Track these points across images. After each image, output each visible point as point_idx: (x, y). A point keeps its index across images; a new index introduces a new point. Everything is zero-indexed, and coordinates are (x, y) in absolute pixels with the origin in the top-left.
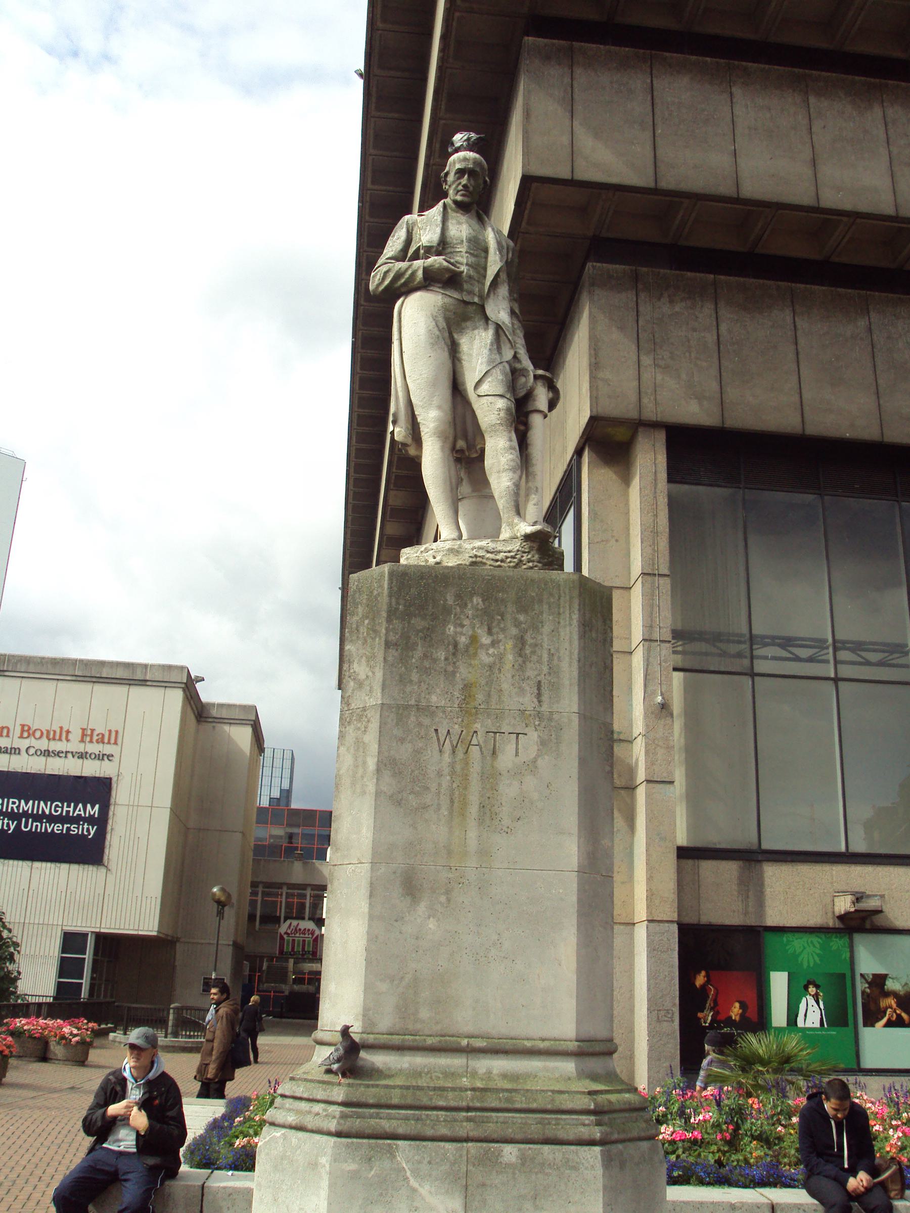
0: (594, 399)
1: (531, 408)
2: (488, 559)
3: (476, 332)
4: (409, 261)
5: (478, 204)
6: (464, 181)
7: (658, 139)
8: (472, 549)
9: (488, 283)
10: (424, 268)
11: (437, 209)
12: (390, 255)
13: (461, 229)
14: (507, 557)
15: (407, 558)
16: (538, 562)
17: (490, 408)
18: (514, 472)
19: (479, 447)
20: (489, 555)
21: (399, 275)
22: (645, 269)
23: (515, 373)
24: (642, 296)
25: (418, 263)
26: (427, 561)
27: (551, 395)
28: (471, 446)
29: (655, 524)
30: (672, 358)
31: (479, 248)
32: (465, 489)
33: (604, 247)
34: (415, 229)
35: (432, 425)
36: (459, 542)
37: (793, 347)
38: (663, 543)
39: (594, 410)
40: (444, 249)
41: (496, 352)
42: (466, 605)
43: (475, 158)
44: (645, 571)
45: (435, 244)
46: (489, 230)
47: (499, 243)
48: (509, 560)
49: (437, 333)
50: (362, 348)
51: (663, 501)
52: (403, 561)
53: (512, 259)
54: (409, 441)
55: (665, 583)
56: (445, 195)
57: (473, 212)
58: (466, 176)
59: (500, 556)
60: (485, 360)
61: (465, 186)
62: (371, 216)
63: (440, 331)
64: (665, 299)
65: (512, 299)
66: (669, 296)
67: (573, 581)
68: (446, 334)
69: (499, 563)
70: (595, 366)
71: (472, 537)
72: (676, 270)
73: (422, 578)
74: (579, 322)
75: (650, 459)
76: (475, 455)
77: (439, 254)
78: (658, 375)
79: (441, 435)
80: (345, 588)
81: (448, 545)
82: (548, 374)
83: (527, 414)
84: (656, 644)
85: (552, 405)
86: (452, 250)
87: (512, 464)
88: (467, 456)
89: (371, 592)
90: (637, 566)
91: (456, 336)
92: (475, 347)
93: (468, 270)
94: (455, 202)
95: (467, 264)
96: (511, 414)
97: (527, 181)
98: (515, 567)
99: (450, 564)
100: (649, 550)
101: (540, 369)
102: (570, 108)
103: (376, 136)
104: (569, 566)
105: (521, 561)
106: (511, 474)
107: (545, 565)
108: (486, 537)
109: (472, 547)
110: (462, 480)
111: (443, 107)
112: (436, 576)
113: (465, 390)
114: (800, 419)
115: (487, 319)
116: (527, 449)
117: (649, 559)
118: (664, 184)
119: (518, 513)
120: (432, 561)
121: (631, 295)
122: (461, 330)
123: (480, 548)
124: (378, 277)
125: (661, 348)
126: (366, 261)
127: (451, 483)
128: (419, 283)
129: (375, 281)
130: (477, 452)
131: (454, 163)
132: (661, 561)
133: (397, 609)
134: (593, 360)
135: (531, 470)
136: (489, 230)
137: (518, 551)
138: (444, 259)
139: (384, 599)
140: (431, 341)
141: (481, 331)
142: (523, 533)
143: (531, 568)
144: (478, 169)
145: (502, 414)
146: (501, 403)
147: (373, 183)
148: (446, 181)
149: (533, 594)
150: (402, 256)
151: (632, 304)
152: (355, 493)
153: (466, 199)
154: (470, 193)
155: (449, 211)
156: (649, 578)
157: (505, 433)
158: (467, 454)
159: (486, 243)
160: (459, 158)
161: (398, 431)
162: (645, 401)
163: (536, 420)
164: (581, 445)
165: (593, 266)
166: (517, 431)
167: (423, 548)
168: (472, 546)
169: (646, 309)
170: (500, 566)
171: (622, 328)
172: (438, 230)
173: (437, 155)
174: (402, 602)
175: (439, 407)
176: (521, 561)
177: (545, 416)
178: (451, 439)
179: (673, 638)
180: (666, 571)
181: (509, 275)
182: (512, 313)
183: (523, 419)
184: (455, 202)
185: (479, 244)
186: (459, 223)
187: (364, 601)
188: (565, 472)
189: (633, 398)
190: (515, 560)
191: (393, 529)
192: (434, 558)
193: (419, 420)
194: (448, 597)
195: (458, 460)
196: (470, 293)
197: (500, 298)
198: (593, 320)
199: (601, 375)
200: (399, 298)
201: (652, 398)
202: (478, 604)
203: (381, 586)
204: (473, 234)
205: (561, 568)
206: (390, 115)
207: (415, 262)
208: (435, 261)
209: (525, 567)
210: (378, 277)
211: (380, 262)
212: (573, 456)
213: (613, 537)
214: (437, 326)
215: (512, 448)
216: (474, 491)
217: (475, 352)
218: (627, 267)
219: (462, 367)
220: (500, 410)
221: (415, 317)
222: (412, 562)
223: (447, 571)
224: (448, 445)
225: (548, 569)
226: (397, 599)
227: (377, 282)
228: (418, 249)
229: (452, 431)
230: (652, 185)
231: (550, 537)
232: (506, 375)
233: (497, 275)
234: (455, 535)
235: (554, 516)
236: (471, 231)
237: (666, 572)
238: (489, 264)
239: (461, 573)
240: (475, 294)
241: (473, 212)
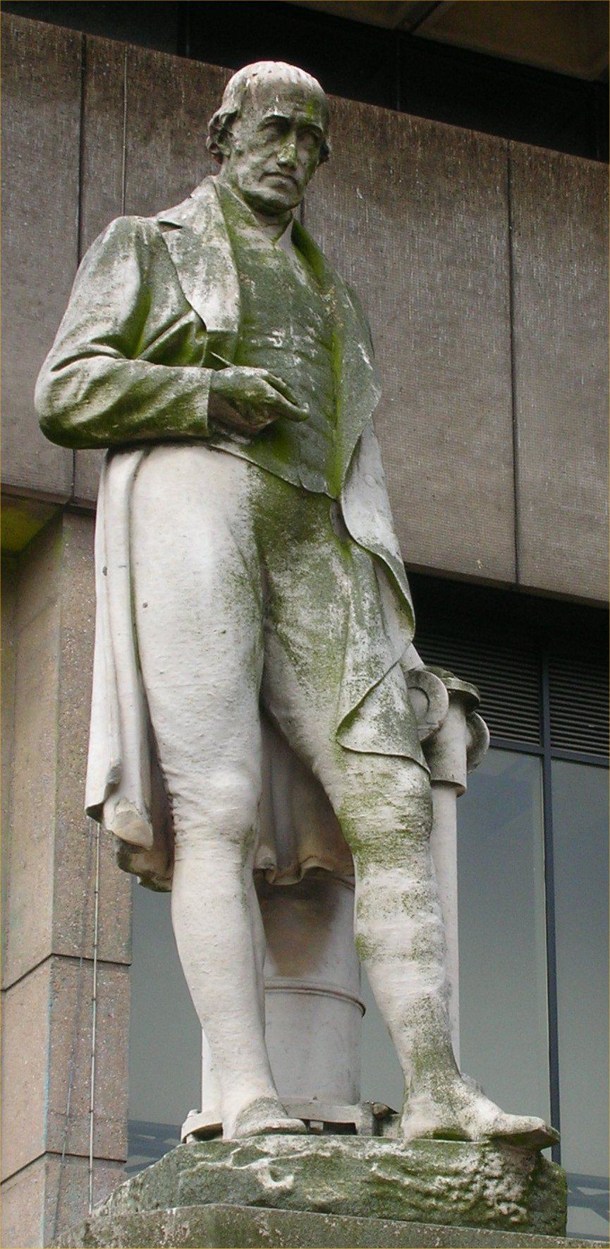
10: (214, 393)
14: (451, 1188)
16: (520, 1203)
20: (407, 1181)
22: (107, 42)
24: (99, 122)
35: (219, 810)
37: (504, 327)
48: (454, 1195)
49: (242, 570)
59: (437, 1184)
64: (161, 144)
72: (193, 57)
84: (83, 1166)
91: (276, 578)
114: (508, 541)
121: (66, 114)
137: (476, 1172)
151: (69, 146)
156: (70, 969)
175: (241, 765)
179: (132, 1151)
190: (469, 1196)
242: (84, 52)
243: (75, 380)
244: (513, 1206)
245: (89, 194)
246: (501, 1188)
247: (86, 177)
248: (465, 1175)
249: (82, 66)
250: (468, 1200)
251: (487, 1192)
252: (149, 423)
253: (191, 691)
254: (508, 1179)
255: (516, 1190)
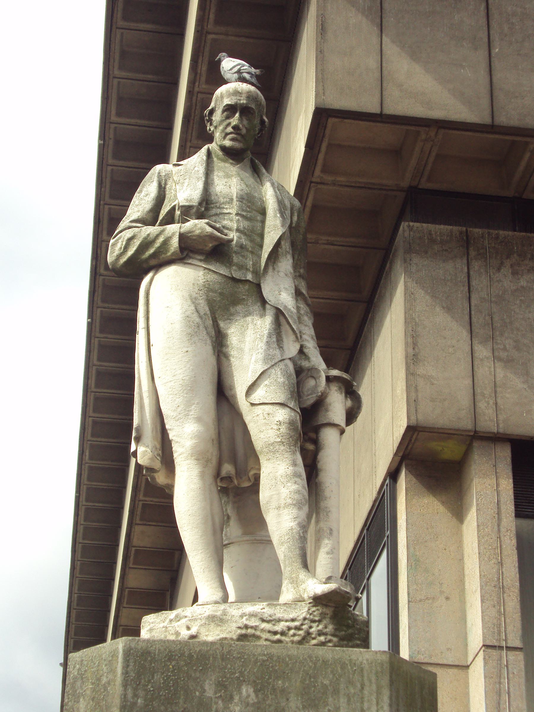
0: (413, 403)
1: (322, 420)
2: (263, 630)
3: (249, 319)
4: (160, 225)
5: (255, 150)
6: (235, 120)
7: (495, 60)
8: (242, 616)
9: (265, 255)
11: (200, 156)
12: (135, 216)
13: (230, 183)
14: (289, 629)
15: (151, 630)
16: (333, 635)
17: (267, 421)
18: (300, 509)
19: (252, 473)
20: (264, 625)
21: (146, 244)
23: (301, 373)
24: (476, 265)
25: (173, 229)
26: (177, 634)
27: (349, 403)
28: (241, 472)
29: (500, 575)
30: (517, 348)
31: (252, 208)
32: (234, 530)
33: (421, 202)
34: (169, 183)
36: (222, 607)
38: (513, 603)
39: (413, 418)
40: (207, 209)
41: (275, 345)
42: (231, 698)
43: (249, 92)
44: (489, 643)
45: (195, 203)
46: (268, 185)
47: (280, 203)
48: (292, 632)
49: (198, 320)
50: (101, 332)
51: (510, 544)
52: (145, 634)
53: (298, 223)
54: (157, 465)
55: (517, 660)
56: (210, 139)
57: (247, 161)
58: (237, 115)
59: (280, 627)
60: (261, 356)
61: (235, 128)
62: (116, 156)
63: (201, 317)
64: (506, 270)
65: (297, 276)
66: (512, 266)
67: (382, 664)
68: (210, 322)
69: (278, 637)
70: (413, 359)
71: (242, 600)
72: (520, 231)
73: (170, 659)
74: (391, 301)
75: (490, 486)
76: (246, 484)
77: (200, 216)
78: (498, 370)
79: (200, 456)
80: (65, 665)
81: (208, 610)
82: (345, 376)
83: (317, 429)
85: (351, 416)
86: (218, 211)
87: (296, 496)
88: (235, 483)
89: (99, 679)
90: (476, 636)
91: (222, 324)
92: (248, 339)
93: (239, 238)
94: (223, 148)
95: (238, 230)
96: (295, 429)
97: (321, 115)
98: (300, 642)
99: (210, 639)
100: (493, 612)
101: (335, 368)
102: (378, 20)
103: (123, 54)
104: (379, 640)
105: (308, 633)
106: (294, 511)
107: (342, 639)
108: (260, 599)
109: (243, 614)
110: (229, 518)
111: (212, 16)
112: (191, 656)
113: (234, 396)
115: (264, 302)
116: (317, 475)
117: (494, 625)
118: (503, 119)
119: (305, 565)
120: (185, 634)
121: (461, 264)
122: (230, 317)
123: (252, 615)
124: (119, 245)
125: (502, 335)
126: (106, 221)
127: (214, 524)
128: (173, 254)
129: (117, 250)
130: (249, 479)
131: (222, 97)
132: (510, 628)
133: (135, 704)
134: (410, 350)
135: (322, 504)
136: (268, 185)
137: (305, 619)
138: (208, 224)
139: (117, 689)
140: (189, 331)
141: (256, 318)
142: (312, 594)
143: (323, 644)
144: (253, 106)
145: (284, 429)
146: (282, 415)
147: (119, 114)
148: (210, 121)
149: (326, 682)
150: (151, 218)
151: (463, 277)
152: (86, 529)
153: (237, 145)
154: (243, 136)
155: (215, 159)
156: (494, 653)
157: (287, 455)
158: (236, 482)
159: (263, 202)
160: (228, 91)
161: (143, 452)
162: (482, 405)
163: (329, 436)
164: (395, 465)
165: (409, 226)
166: (304, 452)
167: (172, 614)
168: (240, 612)
169: (480, 282)
170: (279, 641)
171: (449, 309)
172: (200, 185)
173: (203, 79)
174: (141, 693)
175: (199, 420)
176: (308, 633)
177: (342, 432)
178: (214, 461)
180: (518, 643)
181: (293, 244)
182: (298, 293)
183: (312, 435)
184: (223, 148)
185: (253, 204)
186: (228, 176)
187: (88, 692)
188: (375, 501)
189: (465, 401)
190: (301, 632)
191: (140, 579)
192: (188, 628)
193: (171, 437)
194: (207, 687)
195: (224, 491)
196: (241, 267)
197: (282, 274)
198: (409, 296)
199: (421, 370)
200: (146, 272)
201: (491, 402)
202: (248, 696)
203: (113, 671)
204: (246, 190)
205: (365, 643)
206: (142, 26)
207: (169, 227)
208: (196, 226)
209: (314, 642)
210: (119, 245)
211: (122, 225)
212: (385, 480)
213: (442, 592)
214: (197, 311)
215: (296, 475)
216: (245, 533)
217: (247, 347)
218: (456, 229)
219: (230, 365)
220: (280, 423)
221: (169, 298)
222: (158, 635)
223: (205, 648)
224: (210, 471)
225: (347, 646)
226: (135, 689)
227: (117, 252)
228: (173, 209)
229: (215, 453)
230: (487, 120)
231: (349, 599)
232: (289, 377)
233: (278, 245)
234: (218, 595)
235: (357, 569)
236: (244, 186)
237: (518, 643)
238: (266, 230)
239: (225, 651)
240: (247, 269)
241: (247, 161)
242: (467, 236)
243: (120, 241)
244: (329, 637)
245: (473, 296)
246: (321, 627)
247: (471, 289)
248: (298, 621)
249: (467, 242)
250: (299, 635)
251: (312, 630)
252: (154, 255)
253: (172, 383)
254: (325, 622)
255: (330, 628)
